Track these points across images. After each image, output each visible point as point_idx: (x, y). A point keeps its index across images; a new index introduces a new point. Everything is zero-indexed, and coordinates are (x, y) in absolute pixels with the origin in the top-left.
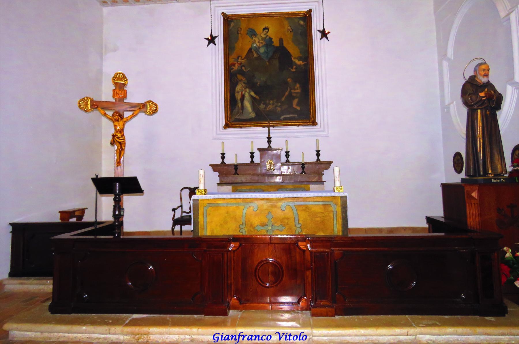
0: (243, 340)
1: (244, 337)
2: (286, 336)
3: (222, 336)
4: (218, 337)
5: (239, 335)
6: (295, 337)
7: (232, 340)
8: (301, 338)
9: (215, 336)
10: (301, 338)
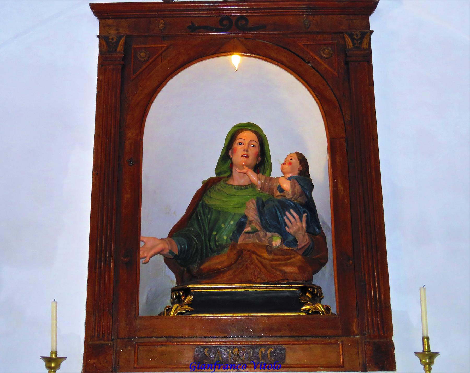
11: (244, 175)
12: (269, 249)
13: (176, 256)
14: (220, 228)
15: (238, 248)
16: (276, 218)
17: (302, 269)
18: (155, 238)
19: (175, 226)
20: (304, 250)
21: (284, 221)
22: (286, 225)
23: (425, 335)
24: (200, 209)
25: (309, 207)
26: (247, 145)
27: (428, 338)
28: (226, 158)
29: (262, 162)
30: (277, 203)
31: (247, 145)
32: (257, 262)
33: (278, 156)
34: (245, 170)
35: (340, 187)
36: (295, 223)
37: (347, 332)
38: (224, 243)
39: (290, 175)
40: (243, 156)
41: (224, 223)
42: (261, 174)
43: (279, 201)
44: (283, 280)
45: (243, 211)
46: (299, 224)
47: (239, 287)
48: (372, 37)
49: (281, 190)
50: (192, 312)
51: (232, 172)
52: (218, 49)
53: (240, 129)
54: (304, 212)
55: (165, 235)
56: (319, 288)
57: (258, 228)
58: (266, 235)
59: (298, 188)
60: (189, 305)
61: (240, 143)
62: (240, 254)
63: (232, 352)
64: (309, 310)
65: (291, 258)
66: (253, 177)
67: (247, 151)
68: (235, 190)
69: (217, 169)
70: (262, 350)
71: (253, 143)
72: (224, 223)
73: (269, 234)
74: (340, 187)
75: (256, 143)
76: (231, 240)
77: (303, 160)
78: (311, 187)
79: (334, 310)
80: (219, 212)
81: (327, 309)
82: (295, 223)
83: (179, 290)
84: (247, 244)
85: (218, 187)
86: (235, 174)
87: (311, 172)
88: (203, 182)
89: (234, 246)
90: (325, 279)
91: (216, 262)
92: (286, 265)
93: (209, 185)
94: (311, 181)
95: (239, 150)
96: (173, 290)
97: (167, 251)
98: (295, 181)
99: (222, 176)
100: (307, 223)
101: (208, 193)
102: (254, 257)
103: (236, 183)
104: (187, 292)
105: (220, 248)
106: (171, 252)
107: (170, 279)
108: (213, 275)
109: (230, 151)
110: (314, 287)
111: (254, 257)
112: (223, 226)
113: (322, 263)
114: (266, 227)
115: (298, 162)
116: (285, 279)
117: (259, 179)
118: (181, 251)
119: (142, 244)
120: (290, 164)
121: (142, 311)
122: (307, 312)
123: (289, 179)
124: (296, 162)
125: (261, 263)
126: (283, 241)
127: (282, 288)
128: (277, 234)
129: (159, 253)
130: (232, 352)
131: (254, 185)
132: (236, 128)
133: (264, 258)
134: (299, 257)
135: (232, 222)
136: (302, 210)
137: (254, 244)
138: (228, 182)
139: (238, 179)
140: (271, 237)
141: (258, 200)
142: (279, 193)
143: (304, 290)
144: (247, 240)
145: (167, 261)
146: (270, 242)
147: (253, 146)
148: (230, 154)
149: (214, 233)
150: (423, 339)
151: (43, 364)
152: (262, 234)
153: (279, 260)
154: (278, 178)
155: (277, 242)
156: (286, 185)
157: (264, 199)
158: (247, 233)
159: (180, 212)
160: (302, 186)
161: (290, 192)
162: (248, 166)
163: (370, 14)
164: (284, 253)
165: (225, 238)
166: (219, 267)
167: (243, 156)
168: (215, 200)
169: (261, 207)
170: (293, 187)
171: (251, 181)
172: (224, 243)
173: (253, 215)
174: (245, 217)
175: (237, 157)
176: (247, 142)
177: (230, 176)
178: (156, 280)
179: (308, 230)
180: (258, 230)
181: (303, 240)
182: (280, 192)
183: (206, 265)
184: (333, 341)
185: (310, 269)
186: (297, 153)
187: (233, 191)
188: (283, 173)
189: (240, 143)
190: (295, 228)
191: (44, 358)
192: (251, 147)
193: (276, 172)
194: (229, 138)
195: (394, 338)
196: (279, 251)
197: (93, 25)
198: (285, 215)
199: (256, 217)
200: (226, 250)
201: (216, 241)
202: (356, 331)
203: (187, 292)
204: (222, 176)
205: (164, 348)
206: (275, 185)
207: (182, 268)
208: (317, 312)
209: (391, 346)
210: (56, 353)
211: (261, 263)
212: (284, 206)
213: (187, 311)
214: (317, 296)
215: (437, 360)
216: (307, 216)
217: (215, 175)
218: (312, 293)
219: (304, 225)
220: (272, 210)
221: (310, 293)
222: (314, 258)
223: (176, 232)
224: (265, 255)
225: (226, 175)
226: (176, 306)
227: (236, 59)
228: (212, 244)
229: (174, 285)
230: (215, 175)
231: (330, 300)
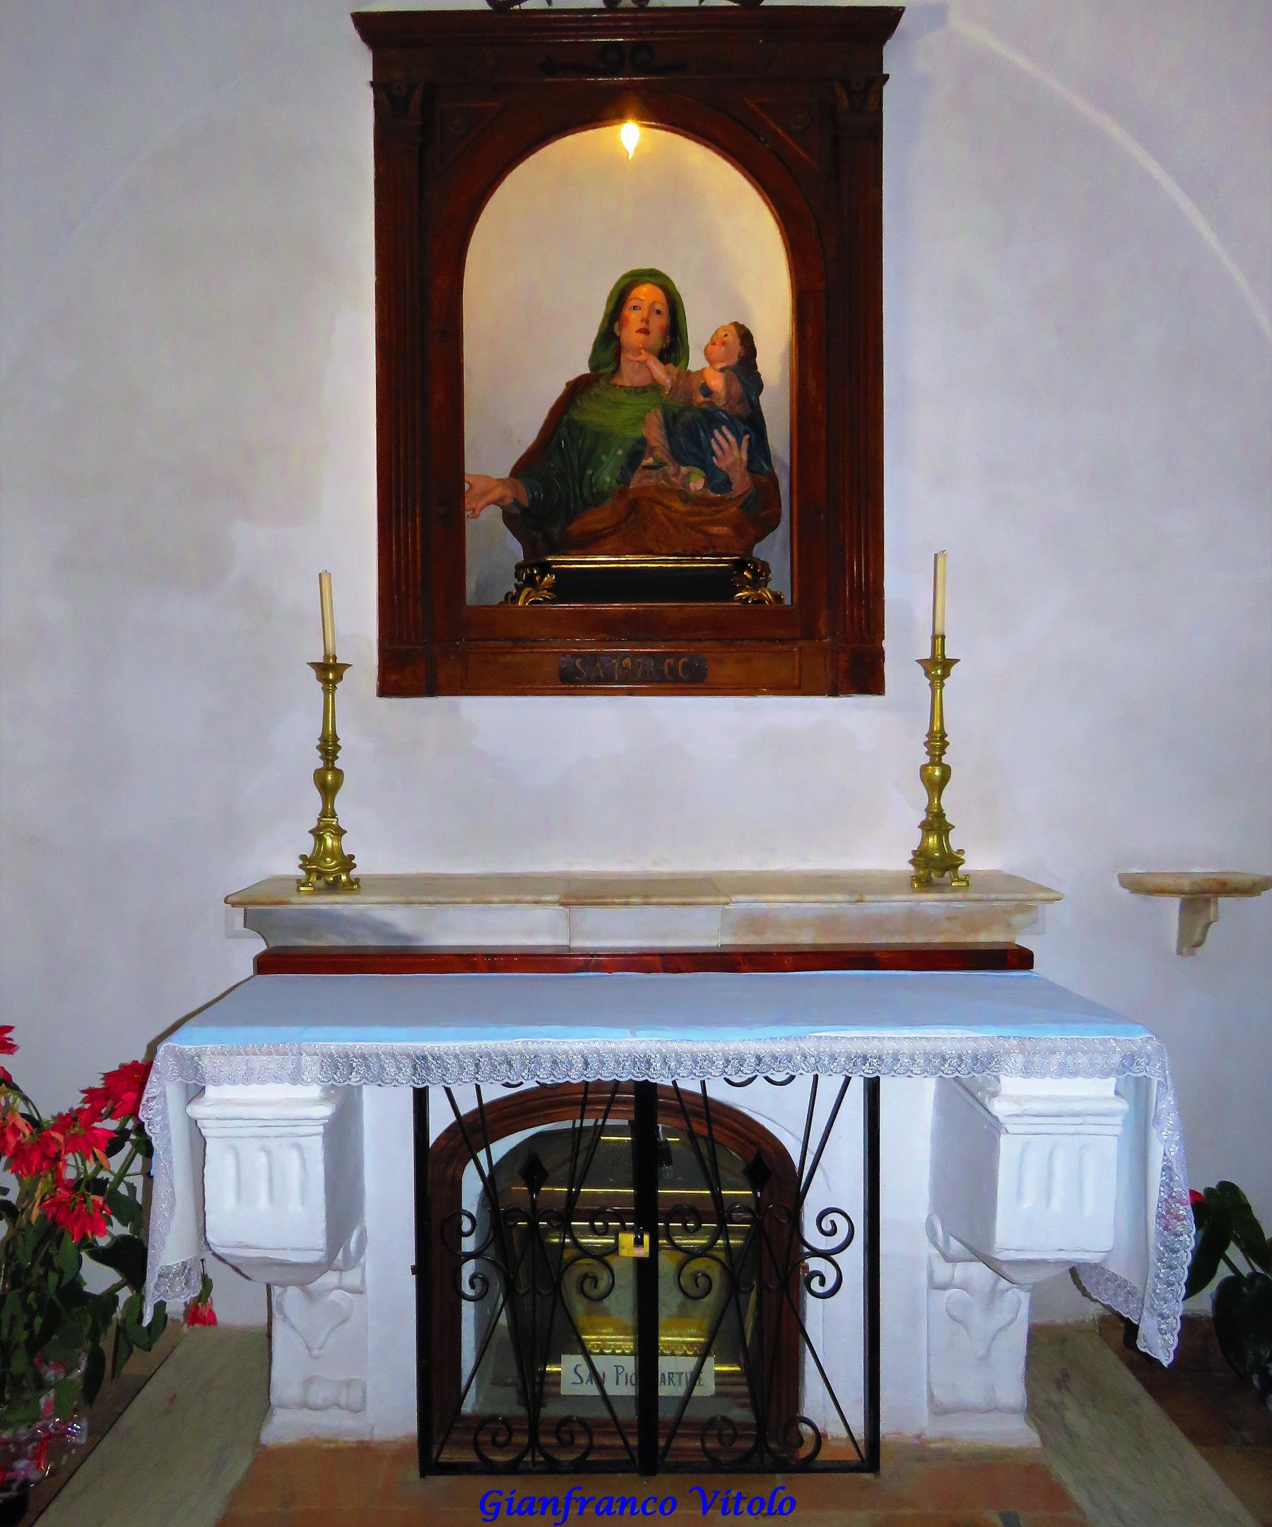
0: (581, 1512)
1: (584, 1503)
2: (726, 1501)
3: (511, 1501)
4: (498, 1505)
5: (568, 1498)
6: (757, 1504)
7: (621, 1513)
8: (776, 1507)
9: (489, 1500)
10: (776, 1507)
11: (643, 365)
12: (686, 497)
13: (525, 511)
14: (601, 462)
15: (631, 496)
16: (698, 443)
17: (738, 529)
18: (488, 478)
19: (521, 459)
20: (741, 501)
21: (710, 446)
22: (713, 454)
23: (938, 632)
24: (563, 430)
25: (754, 424)
26: (644, 313)
27: (943, 637)
28: (609, 341)
29: (673, 344)
30: (699, 414)
31: (644, 313)
32: (662, 518)
33: (701, 329)
34: (642, 358)
35: (811, 382)
36: (729, 451)
37: (810, 633)
38: (606, 488)
39: (724, 365)
40: (639, 331)
41: (607, 453)
42: (671, 366)
43: (704, 411)
44: (706, 548)
45: (642, 431)
46: (736, 453)
47: (632, 561)
48: (887, 90)
49: (707, 391)
50: (554, 601)
51: (619, 363)
52: (597, 112)
53: (633, 282)
54: (746, 433)
55: (504, 471)
56: (765, 564)
57: (666, 460)
58: (679, 471)
59: (737, 387)
60: (549, 590)
61: (635, 308)
62: (634, 505)
63: (621, 664)
64: (748, 598)
65: (719, 512)
66: (659, 371)
67: (647, 322)
68: (625, 395)
69: (591, 361)
70: (668, 661)
71: (658, 307)
72: (607, 453)
73: (684, 469)
74: (811, 382)
75: (662, 305)
76: (618, 482)
77: (746, 337)
78: (759, 386)
79: (787, 601)
80: (597, 435)
81: (778, 598)
82: (729, 451)
83: (532, 567)
84: (646, 488)
85: (595, 390)
86: (626, 367)
87: (759, 360)
88: (568, 384)
89: (622, 493)
90: (775, 550)
91: (594, 519)
92: (714, 523)
93: (577, 389)
94: (759, 375)
95: (634, 319)
96: (519, 567)
97: (509, 500)
98: (732, 373)
99: (602, 371)
100: (749, 452)
101: (578, 402)
102: (658, 509)
103: (626, 383)
104: (545, 568)
105: (598, 498)
106: (516, 502)
107: (515, 550)
108: (589, 543)
109: (616, 325)
110: (756, 562)
111: (658, 509)
112: (604, 459)
113: (769, 525)
114: (679, 457)
115: (738, 341)
116: (709, 546)
117: (668, 373)
118: (533, 501)
119: (467, 487)
120: (724, 344)
121: (471, 598)
122: (744, 601)
123: (722, 370)
124: (733, 339)
125: (670, 520)
126: (709, 482)
127: (705, 561)
128: (697, 470)
129: (495, 503)
130: (621, 664)
131: (659, 385)
132: (628, 280)
133: (676, 511)
134: (734, 509)
135: (620, 452)
136: (742, 428)
137: (659, 488)
138: (613, 382)
139: (630, 375)
140: (688, 476)
141: (666, 410)
142: (701, 398)
143: (740, 565)
144: (645, 481)
145: (508, 519)
146: (686, 485)
147: (659, 312)
148: (616, 330)
149: (590, 472)
150: (934, 638)
151: (312, 673)
152: (671, 469)
153: (700, 514)
154: (701, 373)
155: (697, 483)
156: (717, 382)
157: (676, 411)
158: (649, 467)
159: (528, 434)
160: (743, 383)
161: (723, 395)
162: (647, 350)
163: (883, 42)
164: (710, 503)
165: (608, 479)
166: (599, 527)
167: (639, 331)
168: (591, 414)
169: (671, 422)
170: (728, 384)
171: (653, 379)
172: (606, 488)
173: (654, 433)
174: (643, 441)
175: (630, 335)
176: (645, 306)
177: (617, 370)
178: (492, 552)
179: (752, 467)
180: (665, 464)
181: (741, 483)
182: (705, 396)
183: (575, 527)
184: (785, 648)
185: (752, 531)
186: (736, 324)
187: (621, 396)
188: (709, 360)
189: (635, 308)
190: (729, 461)
191: (313, 665)
192: (654, 315)
193: (696, 361)
194: (615, 298)
195: (885, 644)
196: (700, 501)
197: (356, 68)
198: (713, 436)
199: (662, 440)
200: (609, 501)
201: (591, 486)
202: (823, 631)
203: (545, 568)
204: (602, 371)
205: (509, 657)
206: (696, 384)
207: (534, 533)
208: (761, 601)
209: (880, 654)
210: (335, 658)
211: (670, 520)
212: (711, 419)
213: (545, 599)
214: (761, 573)
215: (954, 670)
216: (750, 440)
217: (588, 371)
218: (753, 572)
219: (744, 456)
220: (690, 425)
221: (750, 571)
222: (759, 516)
223: (526, 467)
224: (678, 505)
225: (609, 370)
226: (526, 590)
227: (630, 135)
228: (586, 490)
229: (521, 557)
230: (588, 371)
231: (780, 582)
